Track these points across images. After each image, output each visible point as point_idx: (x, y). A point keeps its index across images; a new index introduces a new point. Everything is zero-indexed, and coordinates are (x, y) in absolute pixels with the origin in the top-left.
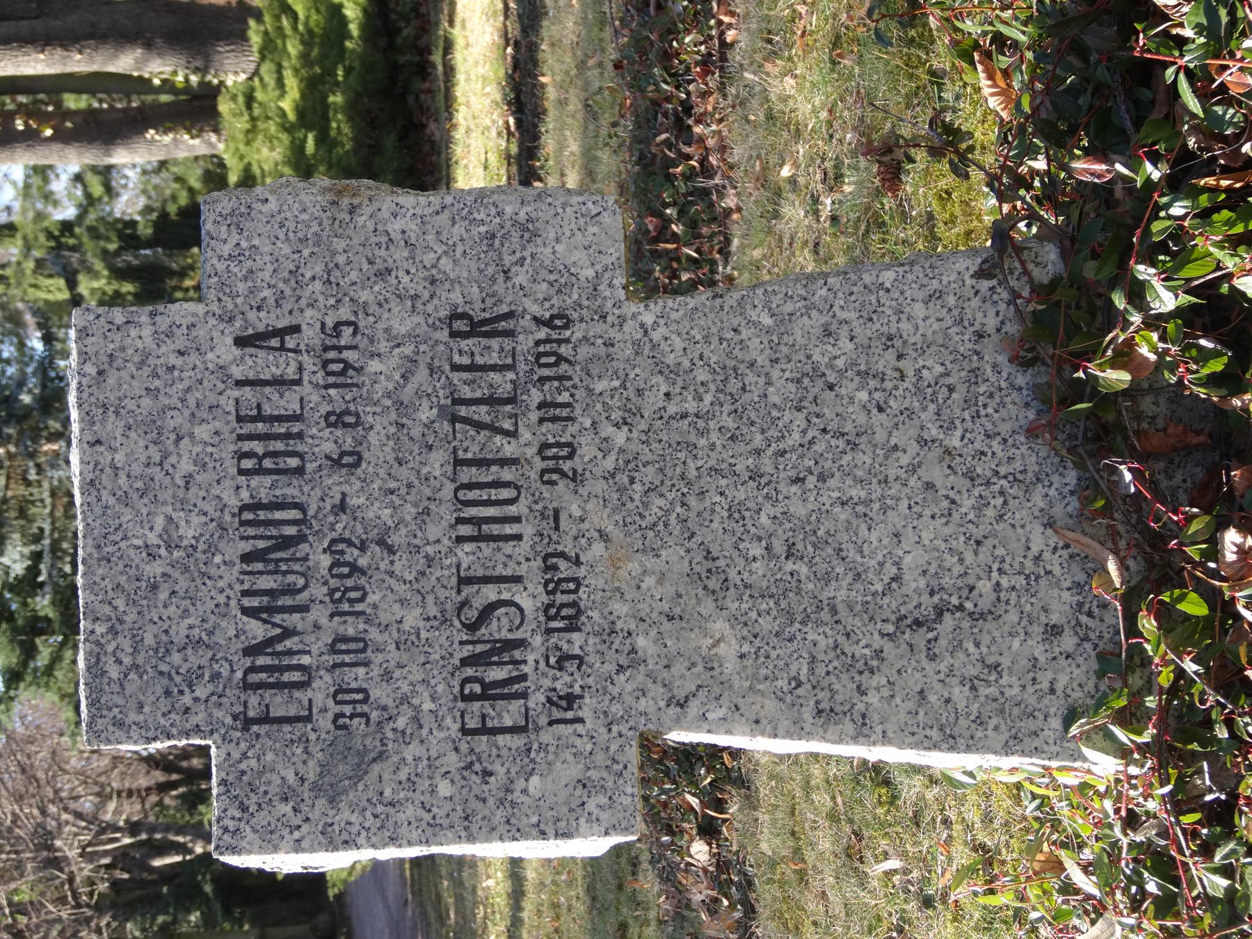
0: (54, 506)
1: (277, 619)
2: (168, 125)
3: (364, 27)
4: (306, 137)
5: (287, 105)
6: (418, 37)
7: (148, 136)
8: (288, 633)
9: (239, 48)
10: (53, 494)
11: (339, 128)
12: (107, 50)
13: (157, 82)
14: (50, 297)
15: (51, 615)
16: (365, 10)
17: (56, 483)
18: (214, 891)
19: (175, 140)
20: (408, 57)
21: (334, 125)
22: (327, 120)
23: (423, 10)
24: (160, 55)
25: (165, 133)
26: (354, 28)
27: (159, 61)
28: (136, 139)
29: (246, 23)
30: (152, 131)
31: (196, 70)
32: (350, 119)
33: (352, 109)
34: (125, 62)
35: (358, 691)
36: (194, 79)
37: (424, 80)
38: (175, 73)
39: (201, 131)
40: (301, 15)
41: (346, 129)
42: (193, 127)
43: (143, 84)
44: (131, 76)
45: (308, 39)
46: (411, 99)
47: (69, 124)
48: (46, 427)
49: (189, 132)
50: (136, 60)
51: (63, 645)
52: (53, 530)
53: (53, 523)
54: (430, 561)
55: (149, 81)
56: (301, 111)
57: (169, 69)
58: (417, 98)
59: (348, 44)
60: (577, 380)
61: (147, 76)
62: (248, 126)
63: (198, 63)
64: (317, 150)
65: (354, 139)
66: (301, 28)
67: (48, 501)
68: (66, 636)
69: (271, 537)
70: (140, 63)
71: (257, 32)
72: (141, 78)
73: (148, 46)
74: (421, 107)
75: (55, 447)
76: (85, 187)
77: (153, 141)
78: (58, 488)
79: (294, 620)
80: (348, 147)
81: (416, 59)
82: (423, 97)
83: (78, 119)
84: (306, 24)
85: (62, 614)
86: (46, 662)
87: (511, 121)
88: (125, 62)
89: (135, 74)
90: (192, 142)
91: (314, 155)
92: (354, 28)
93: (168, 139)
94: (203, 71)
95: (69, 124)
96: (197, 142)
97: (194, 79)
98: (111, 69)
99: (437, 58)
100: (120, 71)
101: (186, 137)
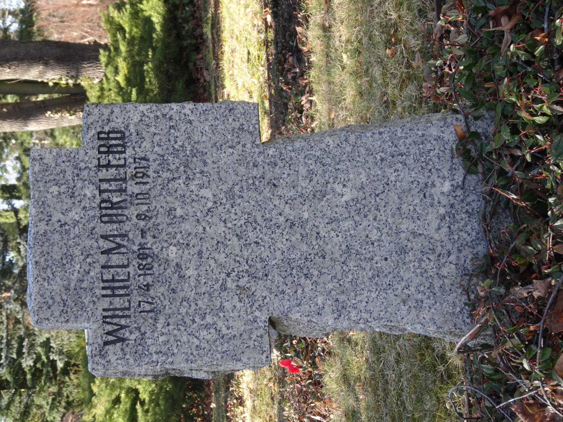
0: (8, 324)
2: (57, 109)
3: (164, 26)
4: (131, 91)
5: (120, 78)
6: (194, 30)
7: (47, 115)
9: (95, 65)
10: (8, 318)
11: (150, 81)
12: (24, 67)
13: (51, 84)
14: (7, 221)
15: (9, 379)
16: (164, 18)
17: (9, 312)
18: (275, 92)
19: (61, 116)
20: (189, 41)
21: (147, 80)
22: (143, 79)
23: (197, 15)
24: (52, 69)
25: (56, 113)
26: (158, 27)
27: (52, 72)
28: (40, 117)
29: (98, 52)
30: (49, 112)
31: (72, 77)
32: (157, 76)
33: (157, 69)
34: (33, 73)
36: (71, 82)
37: (198, 54)
38: (61, 79)
39: (75, 111)
40: (127, 29)
41: (154, 81)
42: (71, 109)
43: (42, 86)
45: (131, 43)
46: (191, 65)
47: (5, 110)
48: (4, 284)
49: (69, 112)
50: (40, 72)
51: (14, 394)
52: (7, 335)
53: (7, 332)
54: (192, 354)
55: (47, 83)
56: (128, 80)
57: (57, 77)
58: (195, 64)
59: (154, 36)
61: (45, 81)
62: (99, 94)
63: (73, 73)
65: (159, 87)
66: (127, 36)
67: (5, 322)
68: (16, 390)
69: (116, 324)
70: (42, 74)
71: (104, 56)
72: (42, 82)
73: (46, 64)
74: (197, 69)
75: (9, 295)
76: (21, 162)
77: (50, 117)
78: (10, 315)
79: (123, 322)
80: (155, 92)
81: (194, 42)
82: (198, 62)
83: (10, 107)
84: (130, 33)
85: (14, 378)
86: (6, 403)
87: (269, 18)
88: (33, 73)
89: (40, 80)
90: (70, 117)
92: (158, 27)
93: (58, 116)
94: (76, 77)
95: (5, 110)
96: (73, 117)
97: (71, 82)
98: (26, 77)
99: (207, 30)
101: (68, 115)
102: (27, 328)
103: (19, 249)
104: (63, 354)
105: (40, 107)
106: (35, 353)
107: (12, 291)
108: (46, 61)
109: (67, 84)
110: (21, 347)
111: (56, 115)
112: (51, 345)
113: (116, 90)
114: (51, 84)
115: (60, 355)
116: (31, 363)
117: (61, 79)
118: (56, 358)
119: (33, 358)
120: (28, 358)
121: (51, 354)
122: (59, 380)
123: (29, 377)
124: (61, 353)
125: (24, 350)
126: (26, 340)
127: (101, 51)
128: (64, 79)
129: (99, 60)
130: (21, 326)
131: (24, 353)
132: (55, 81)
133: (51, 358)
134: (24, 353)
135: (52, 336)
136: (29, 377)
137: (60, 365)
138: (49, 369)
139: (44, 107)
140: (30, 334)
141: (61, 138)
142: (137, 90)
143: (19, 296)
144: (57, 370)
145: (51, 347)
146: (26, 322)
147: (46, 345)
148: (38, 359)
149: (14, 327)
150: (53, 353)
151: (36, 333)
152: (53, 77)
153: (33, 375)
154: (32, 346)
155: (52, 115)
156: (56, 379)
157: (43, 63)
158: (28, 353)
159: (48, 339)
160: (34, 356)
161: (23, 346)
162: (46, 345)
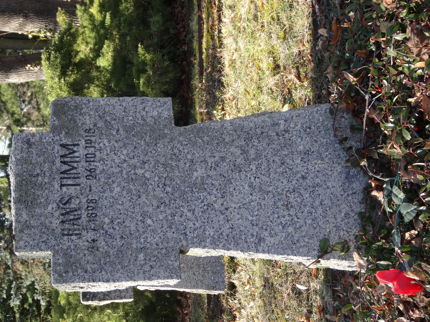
1: (72, 164)
7: (27, 68)
8: (74, 168)
13: (30, 36)
27: (16, 76)
29: (75, 7)
30: (29, 66)
31: (50, 30)
35: (92, 154)
38: (40, 32)
44: (17, 34)
55: (27, 36)
60: (215, 221)
61: (25, 33)
63: (51, 27)
64: (112, 22)
69: (70, 174)
70: (21, 26)
72: (22, 35)
73: (26, 17)
77: (29, 70)
89: (20, 33)
91: (110, 26)
100: (12, 31)
102: (15, 273)
103: (10, 206)
104: (46, 294)
105: (21, 61)
106: (21, 294)
107: (3, 242)
108: (26, 13)
109: (46, 37)
110: (10, 288)
111: (35, 68)
112: (36, 287)
113: (90, 27)
114: (30, 36)
115: (42, 295)
116: (18, 303)
117: (40, 32)
118: (39, 298)
119: (20, 299)
120: (15, 299)
121: (35, 294)
122: (43, 318)
123: (17, 315)
124: (44, 293)
125: (12, 292)
126: (14, 283)
127: (78, 6)
128: (42, 32)
129: (76, 15)
130: (10, 271)
131: (12, 295)
132: (34, 34)
133: (36, 298)
134: (12, 295)
135: (36, 280)
136: (17, 315)
137: (43, 303)
138: (35, 309)
139: (25, 60)
140: (18, 277)
141: (46, 110)
142: (111, 14)
143: (8, 245)
144: (40, 309)
145: (36, 289)
146: (15, 268)
147: (32, 288)
148: (24, 300)
149: (5, 271)
150: (37, 294)
151: (23, 277)
152: (33, 30)
153: (21, 314)
154: (19, 288)
155: (31, 68)
156: (40, 316)
157: (23, 16)
158: (16, 294)
159: (33, 283)
160: (21, 296)
161: (11, 288)
162: (32, 288)
